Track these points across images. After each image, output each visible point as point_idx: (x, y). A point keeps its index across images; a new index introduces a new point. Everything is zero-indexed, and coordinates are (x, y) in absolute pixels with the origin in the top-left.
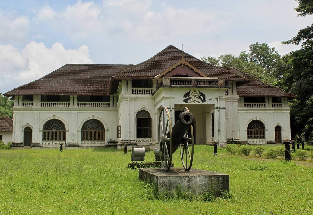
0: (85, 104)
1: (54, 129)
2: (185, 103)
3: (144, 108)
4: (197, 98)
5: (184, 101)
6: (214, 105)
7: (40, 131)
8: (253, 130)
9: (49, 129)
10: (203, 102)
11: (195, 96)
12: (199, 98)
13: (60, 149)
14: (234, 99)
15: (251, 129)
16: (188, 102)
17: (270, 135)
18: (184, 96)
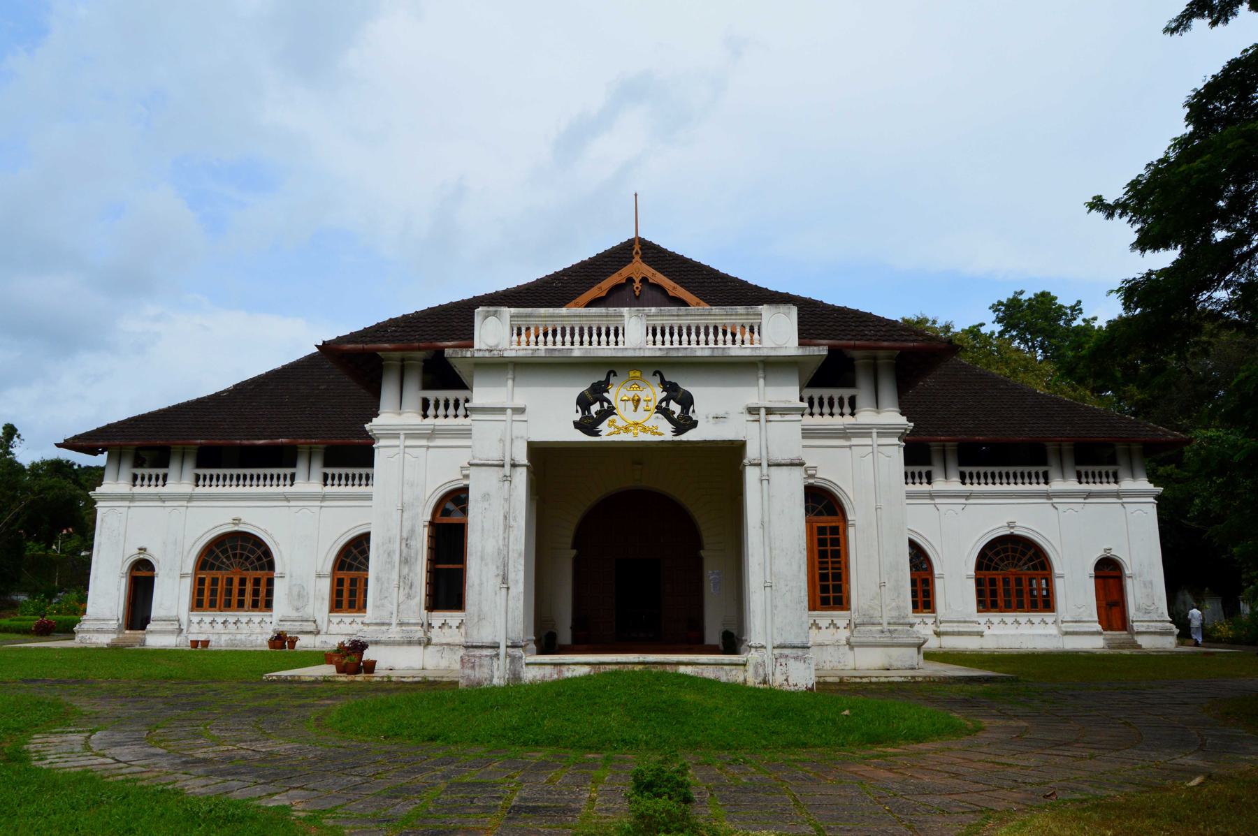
2: (580, 437)
5: (578, 425)
8: (998, 575)
9: (219, 568)
10: (679, 431)
12: (659, 409)
14: (884, 431)
16: (597, 434)
17: (1075, 591)
18: (578, 403)
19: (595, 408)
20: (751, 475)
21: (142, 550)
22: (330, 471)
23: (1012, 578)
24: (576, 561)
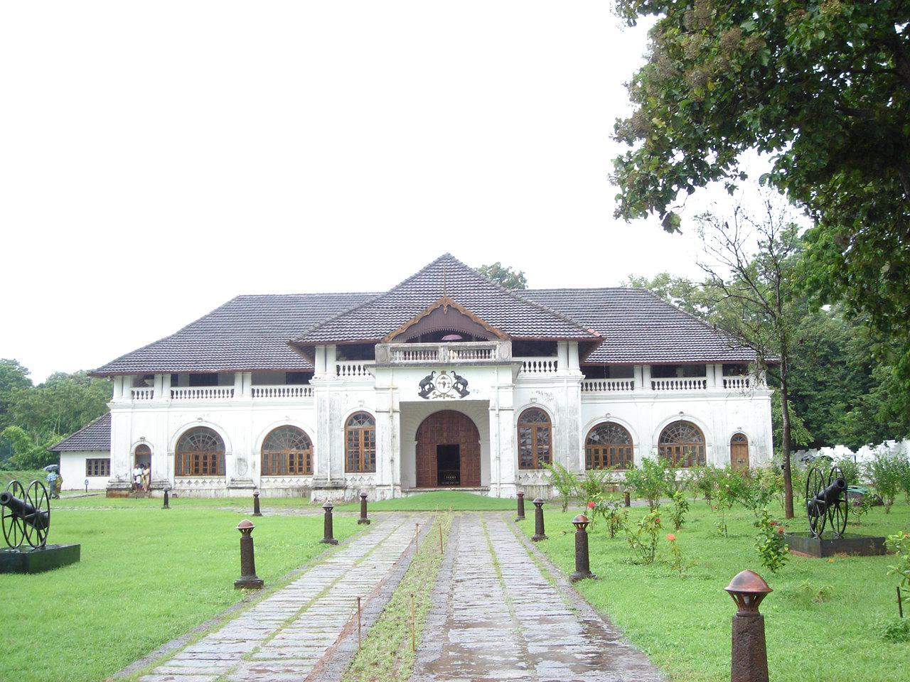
0: (282, 390)
1: (201, 452)
2: (421, 399)
4: (449, 387)
5: (420, 394)
6: (486, 403)
7: (131, 454)
10: (462, 397)
11: (444, 384)
13: (162, 502)
15: (669, 443)
16: (428, 398)
20: (492, 414)
21: (143, 439)
24: (418, 447)
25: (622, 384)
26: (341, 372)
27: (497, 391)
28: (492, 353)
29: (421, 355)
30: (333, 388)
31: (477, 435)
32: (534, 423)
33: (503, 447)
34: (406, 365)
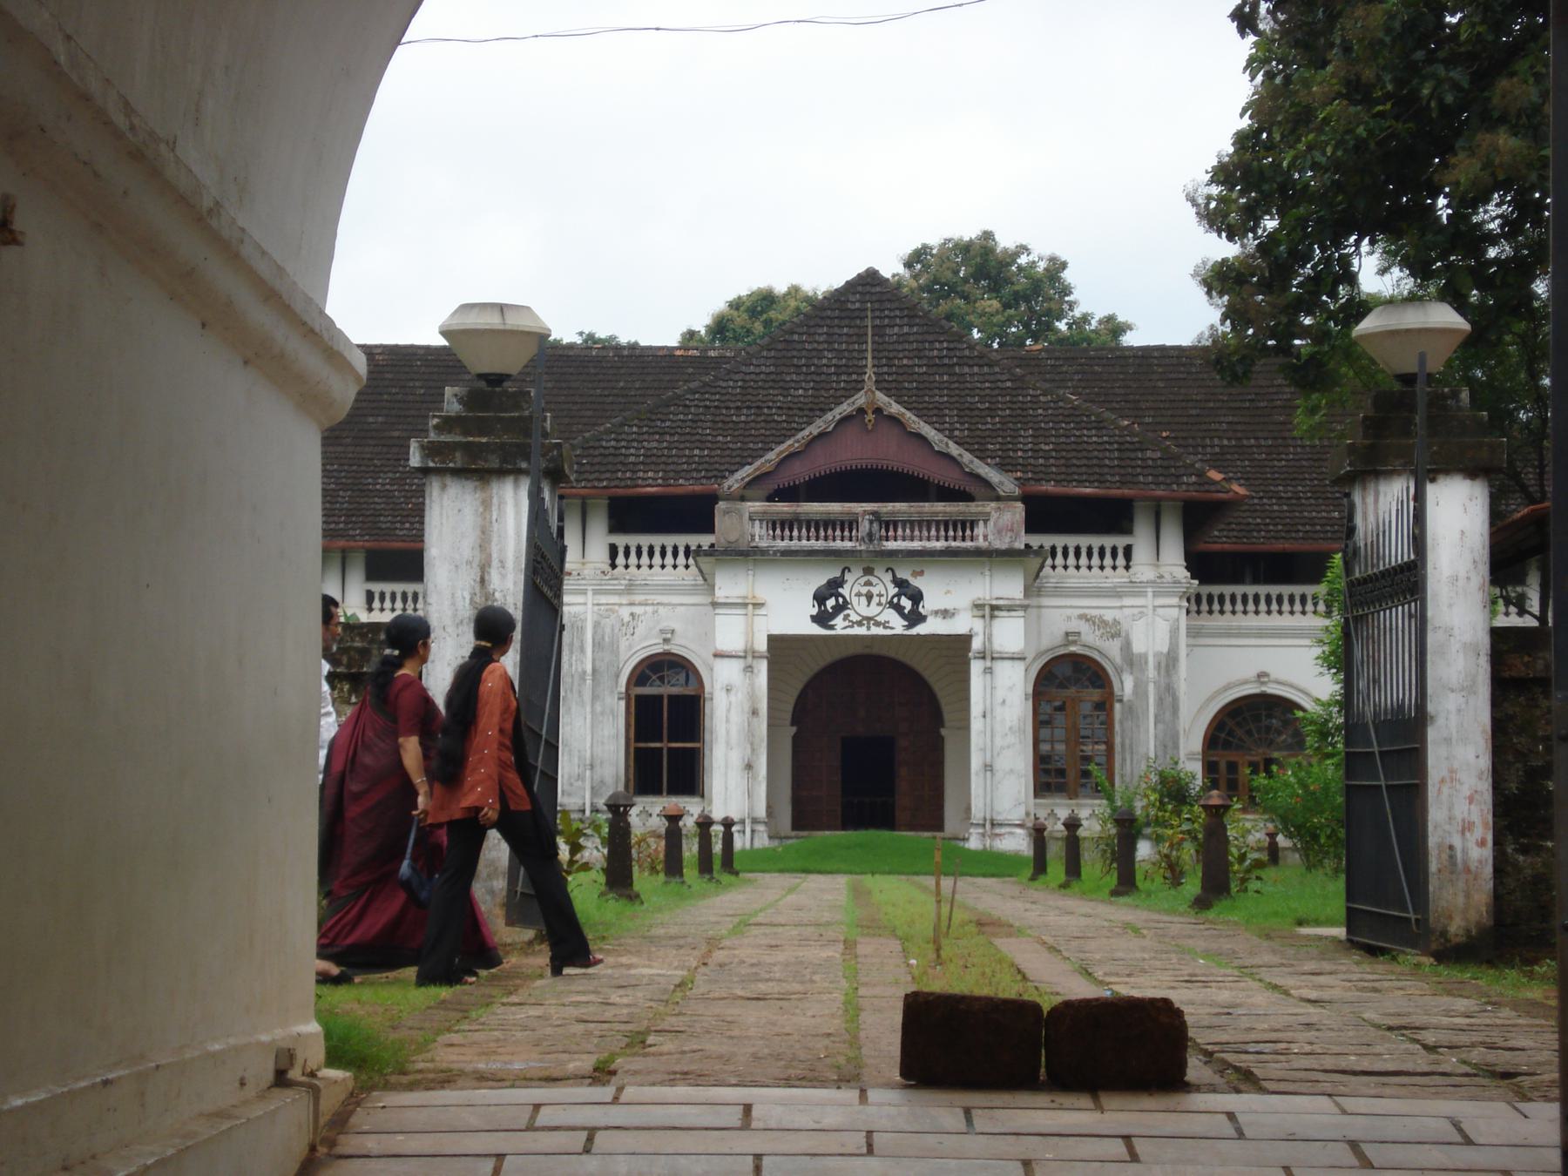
2: (816, 630)
3: (666, 641)
4: (879, 604)
5: (814, 619)
10: (909, 627)
11: (869, 597)
16: (832, 627)
19: (831, 603)
20: (976, 667)
22: (377, 587)
23: (1223, 766)
24: (795, 738)
25: (1245, 598)
26: (620, 560)
27: (993, 620)
28: (980, 530)
29: (817, 530)
30: (603, 599)
31: (937, 718)
32: (1072, 687)
33: (999, 741)
34: (787, 553)
